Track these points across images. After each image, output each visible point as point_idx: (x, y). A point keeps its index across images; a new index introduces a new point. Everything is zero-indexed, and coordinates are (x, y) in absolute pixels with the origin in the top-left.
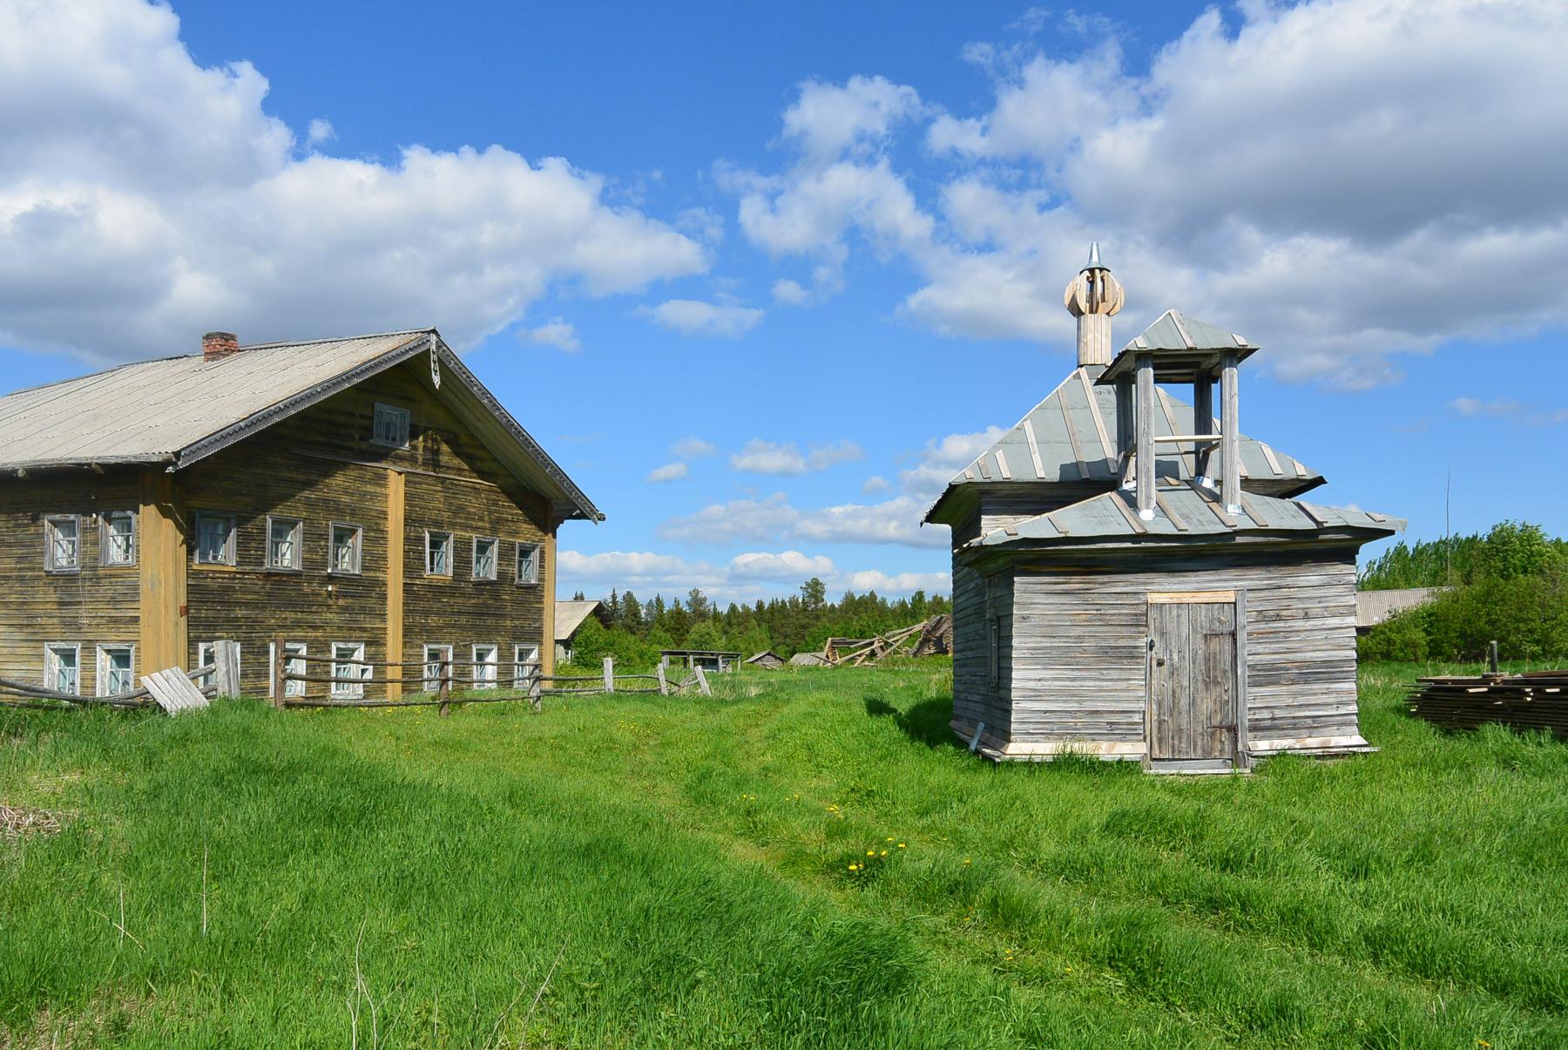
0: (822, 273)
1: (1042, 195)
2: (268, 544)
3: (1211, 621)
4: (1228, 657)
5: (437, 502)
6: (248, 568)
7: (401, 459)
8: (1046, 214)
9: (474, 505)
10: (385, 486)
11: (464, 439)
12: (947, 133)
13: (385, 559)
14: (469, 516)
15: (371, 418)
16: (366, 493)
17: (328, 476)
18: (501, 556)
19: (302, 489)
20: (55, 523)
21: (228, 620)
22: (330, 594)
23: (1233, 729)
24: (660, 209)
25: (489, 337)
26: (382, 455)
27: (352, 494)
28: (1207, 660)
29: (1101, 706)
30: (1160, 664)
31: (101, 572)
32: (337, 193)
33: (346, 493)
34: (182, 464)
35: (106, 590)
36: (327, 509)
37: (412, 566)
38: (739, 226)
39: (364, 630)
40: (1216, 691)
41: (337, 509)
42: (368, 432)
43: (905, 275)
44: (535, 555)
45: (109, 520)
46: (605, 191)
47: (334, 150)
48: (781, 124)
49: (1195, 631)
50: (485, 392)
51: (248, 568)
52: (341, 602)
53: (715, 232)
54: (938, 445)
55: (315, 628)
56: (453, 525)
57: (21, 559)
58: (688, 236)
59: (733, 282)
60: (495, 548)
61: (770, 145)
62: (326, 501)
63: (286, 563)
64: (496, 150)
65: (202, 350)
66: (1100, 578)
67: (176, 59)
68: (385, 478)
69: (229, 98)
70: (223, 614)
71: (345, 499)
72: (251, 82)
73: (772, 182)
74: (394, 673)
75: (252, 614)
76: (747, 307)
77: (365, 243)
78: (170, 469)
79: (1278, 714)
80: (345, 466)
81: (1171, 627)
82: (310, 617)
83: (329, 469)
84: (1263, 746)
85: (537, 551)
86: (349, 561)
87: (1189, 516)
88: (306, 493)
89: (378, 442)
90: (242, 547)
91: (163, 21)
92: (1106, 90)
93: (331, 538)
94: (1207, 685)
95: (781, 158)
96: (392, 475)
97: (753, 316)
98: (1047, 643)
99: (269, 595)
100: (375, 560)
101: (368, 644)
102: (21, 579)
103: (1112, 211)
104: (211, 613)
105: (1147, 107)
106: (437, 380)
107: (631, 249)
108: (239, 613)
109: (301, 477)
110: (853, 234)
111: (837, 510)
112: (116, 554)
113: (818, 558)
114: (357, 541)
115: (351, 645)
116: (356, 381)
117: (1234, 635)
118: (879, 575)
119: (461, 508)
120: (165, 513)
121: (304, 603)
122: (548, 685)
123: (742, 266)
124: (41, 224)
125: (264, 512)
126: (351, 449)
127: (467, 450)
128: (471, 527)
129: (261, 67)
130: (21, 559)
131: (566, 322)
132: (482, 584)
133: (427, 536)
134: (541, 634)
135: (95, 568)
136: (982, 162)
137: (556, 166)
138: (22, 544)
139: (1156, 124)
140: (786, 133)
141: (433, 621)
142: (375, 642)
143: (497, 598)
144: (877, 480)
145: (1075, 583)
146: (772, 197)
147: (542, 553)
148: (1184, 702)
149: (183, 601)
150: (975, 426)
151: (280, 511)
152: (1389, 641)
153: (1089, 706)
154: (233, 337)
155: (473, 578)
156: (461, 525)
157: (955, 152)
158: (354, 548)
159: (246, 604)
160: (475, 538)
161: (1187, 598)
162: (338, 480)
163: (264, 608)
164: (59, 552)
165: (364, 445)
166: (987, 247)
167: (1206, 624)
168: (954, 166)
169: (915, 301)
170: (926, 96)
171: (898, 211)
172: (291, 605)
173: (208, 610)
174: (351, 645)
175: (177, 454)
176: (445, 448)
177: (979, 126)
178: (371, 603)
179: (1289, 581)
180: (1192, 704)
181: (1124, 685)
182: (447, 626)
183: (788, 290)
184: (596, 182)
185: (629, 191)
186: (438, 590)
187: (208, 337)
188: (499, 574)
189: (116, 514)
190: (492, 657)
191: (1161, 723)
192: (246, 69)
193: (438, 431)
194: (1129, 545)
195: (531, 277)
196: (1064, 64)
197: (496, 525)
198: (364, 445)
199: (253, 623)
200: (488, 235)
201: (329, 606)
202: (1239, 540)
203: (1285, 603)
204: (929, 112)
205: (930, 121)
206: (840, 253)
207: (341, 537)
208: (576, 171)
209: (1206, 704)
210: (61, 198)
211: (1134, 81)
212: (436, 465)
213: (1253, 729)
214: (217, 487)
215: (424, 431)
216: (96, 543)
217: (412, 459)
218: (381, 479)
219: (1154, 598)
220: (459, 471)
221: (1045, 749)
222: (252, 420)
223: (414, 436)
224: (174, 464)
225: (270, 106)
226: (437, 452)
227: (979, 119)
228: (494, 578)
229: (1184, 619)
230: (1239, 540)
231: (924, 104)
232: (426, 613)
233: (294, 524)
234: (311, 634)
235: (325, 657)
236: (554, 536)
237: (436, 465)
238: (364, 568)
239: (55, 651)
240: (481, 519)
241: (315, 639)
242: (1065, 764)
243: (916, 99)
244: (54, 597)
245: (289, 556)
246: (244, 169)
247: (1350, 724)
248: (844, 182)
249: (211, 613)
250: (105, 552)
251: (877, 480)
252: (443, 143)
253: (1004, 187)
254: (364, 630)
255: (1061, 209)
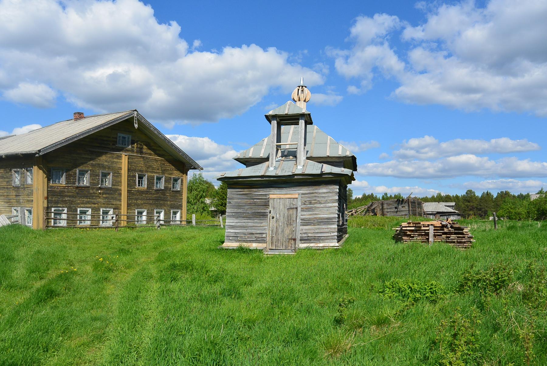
0: (364, 83)
1: (445, 53)
2: (77, 178)
3: (290, 204)
4: (295, 216)
5: (141, 164)
6: (70, 185)
7: (128, 151)
8: (448, 60)
9: (155, 165)
10: (121, 159)
11: (152, 144)
12: (411, 33)
13: (121, 182)
14: (153, 169)
15: (116, 138)
16: (114, 162)
17: (99, 156)
18: (165, 181)
19: (90, 161)
20: (15, 172)
21: (63, 201)
22: (100, 193)
23: (295, 240)
24: (307, 64)
25: (251, 107)
26: (121, 150)
27: (109, 162)
28: (288, 217)
29: (253, 231)
30: (273, 218)
31: (25, 186)
32: (202, 63)
33: (106, 162)
34: (41, 154)
35: (26, 192)
36: (99, 167)
37: (130, 184)
38: (334, 68)
39: (113, 204)
40: (290, 227)
41: (103, 167)
42: (115, 143)
43: (394, 83)
44: (179, 181)
45: (27, 171)
46: (289, 58)
47: (201, 50)
48: (349, 33)
49: (284, 207)
50: (156, 129)
51: (70, 185)
52: (104, 196)
53: (326, 71)
54: (407, 142)
55: (95, 204)
56: (147, 171)
57: (7, 182)
58: (316, 72)
59: (332, 87)
60: (163, 179)
61: (346, 40)
62: (98, 164)
63: (85, 183)
64: (253, 46)
65: (73, 118)
66: (254, 190)
67: (153, 21)
68: (121, 157)
69: (169, 33)
70: (61, 199)
71: (106, 164)
72: (175, 28)
73: (345, 52)
74: (124, 218)
75: (71, 199)
76: (337, 95)
77: (211, 79)
78: (37, 155)
79: (310, 235)
80: (106, 153)
81: (276, 206)
82: (93, 200)
83: (100, 154)
84: (303, 245)
85: (180, 180)
86: (108, 183)
87: (287, 168)
88: (91, 162)
89: (119, 145)
90: (67, 178)
91: (147, 11)
92: (469, 14)
93: (101, 176)
94: (287, 225)
95: (349, 44)
96: (123, 156)
97: (339, 98)
98: (236, 210)
99: (77, 193)
100: (117, 182)
101: (114, 209)
102: (7, 188)
103: (472, 58)
104: (56, 199)
105: (485, 20)
106: (136, 126)
107: (295, 76)
108: (66, 199)
109: (90, 157)
110: (375, 69)
111: (371, 165)
112: (29, 181)
113: (363, 181)
114: (110, 177)
115: (108, 209)
116: (106, 127)
117: (297, 208)
118: (385, 187)
119: (150, 166)
120: (40, 168)
121: (90, 196)
122: (162, 222)
123: (335, 81)
124: (114, 77)
125: (76, 168)
126: (108, 148)
127: (153, 147)
128: (154, 172)
129: (179, 23)
130: (7, 182)
131: (275, 104)
132: (158, 191)
133: (137, 175)
134: (182, 206)
135: (24, 185)
136: (422, 41)
137: (272, 50)
138: (7, 178)
139: (491, 24)
140: (351, 36)
141: (139, 202)
142: (117, 208)
143: (164, 195)
144: (384, 154)
145: (246, 191)
146: (347, 58)
147: (182, 181)
148: (280, 230)
149: (46, 195)
150: (420, 135)
151: (82, 168)
152: (510, 212)
153: (250, 231)
154: (82, 114)
155: (155, 188)
156: (150, 171)
157: (413, 39)
158: (109, 179)
159: (69, 196)
160: (155, 175)
161: (282, 196)
162: (104, 158)
163: (76, 197)
164: (17, 180)
165: (114, 147)
166: (423, 72)
167: (288, 205)
168: (413, 44)
169: (398, 91)
170: (401, 18)
171: (392, 61)
172: (86, 197)
173: (54, 198)
174: (108, 209)
175: (39, 151)
176: (145, 147)
177: (422, 29)
178: (116, 196)
179: (316, 191)
180: (283, 231)
181: (259, 225)
182: (145, 203)
183: (352, 89)
184: (285, 55)
185: (297, 58)
186: (141, 192)
187: (75, 114)
188: (165, 187)
189: (29, 169)
190: (145, 213)
191: (272, 237)
192: (174, 24)
193: (142, 142)
194: (301, 177)
195: (264, 88)
196: (453, 7)
197: (164, 172)
198: (114, 147)
199: (72, 202)
200: (250, 75)
201: (100, 197)
202: (296, 177)
203: (315, 198)
204: (402, 24)
205: (403, 28)
206: (371, 76)
207: (105, 175)
208: (278, 51)
209: (287, 231)
210: (120, 69)
211: (481, 10)
212: (141, 153)
213: (301, 240)
214: (58, 160)
215: (137, 142)
216: (24, 178)
217: (132, 151)
218: (119, 157)
219: (271, 196)
220: (150, 154)
221: (235, 245)
222: (67, 140)
223: (133, 143)
224: (38, 154)
225: (182, 35)
226: (142, 148)
227: (422, 26)
228: (163, 188)
229: (281, 204)
230: (296, 177)
231: (400, 21)
232: (137, 199)
233: (87, 172)
234: (93, 206)
235: (75, 213)
236: (187, 175)
237: (141, 153)
238: (113, 185)
239: (27, 210)
240: (158, 169)
241: (95, 207)
242: (241, 250)
243: (398, 20)
244: (14, 194)
245: (86, 181)
246: (173, 56)
247: (334, 239)
248: (372, 51)
249: (56, 199)
250: (26, 180)
251: (384, 154)
252: (237, 44)
253: (432, 50)
254: (113, 204)
255: (452, 58)
